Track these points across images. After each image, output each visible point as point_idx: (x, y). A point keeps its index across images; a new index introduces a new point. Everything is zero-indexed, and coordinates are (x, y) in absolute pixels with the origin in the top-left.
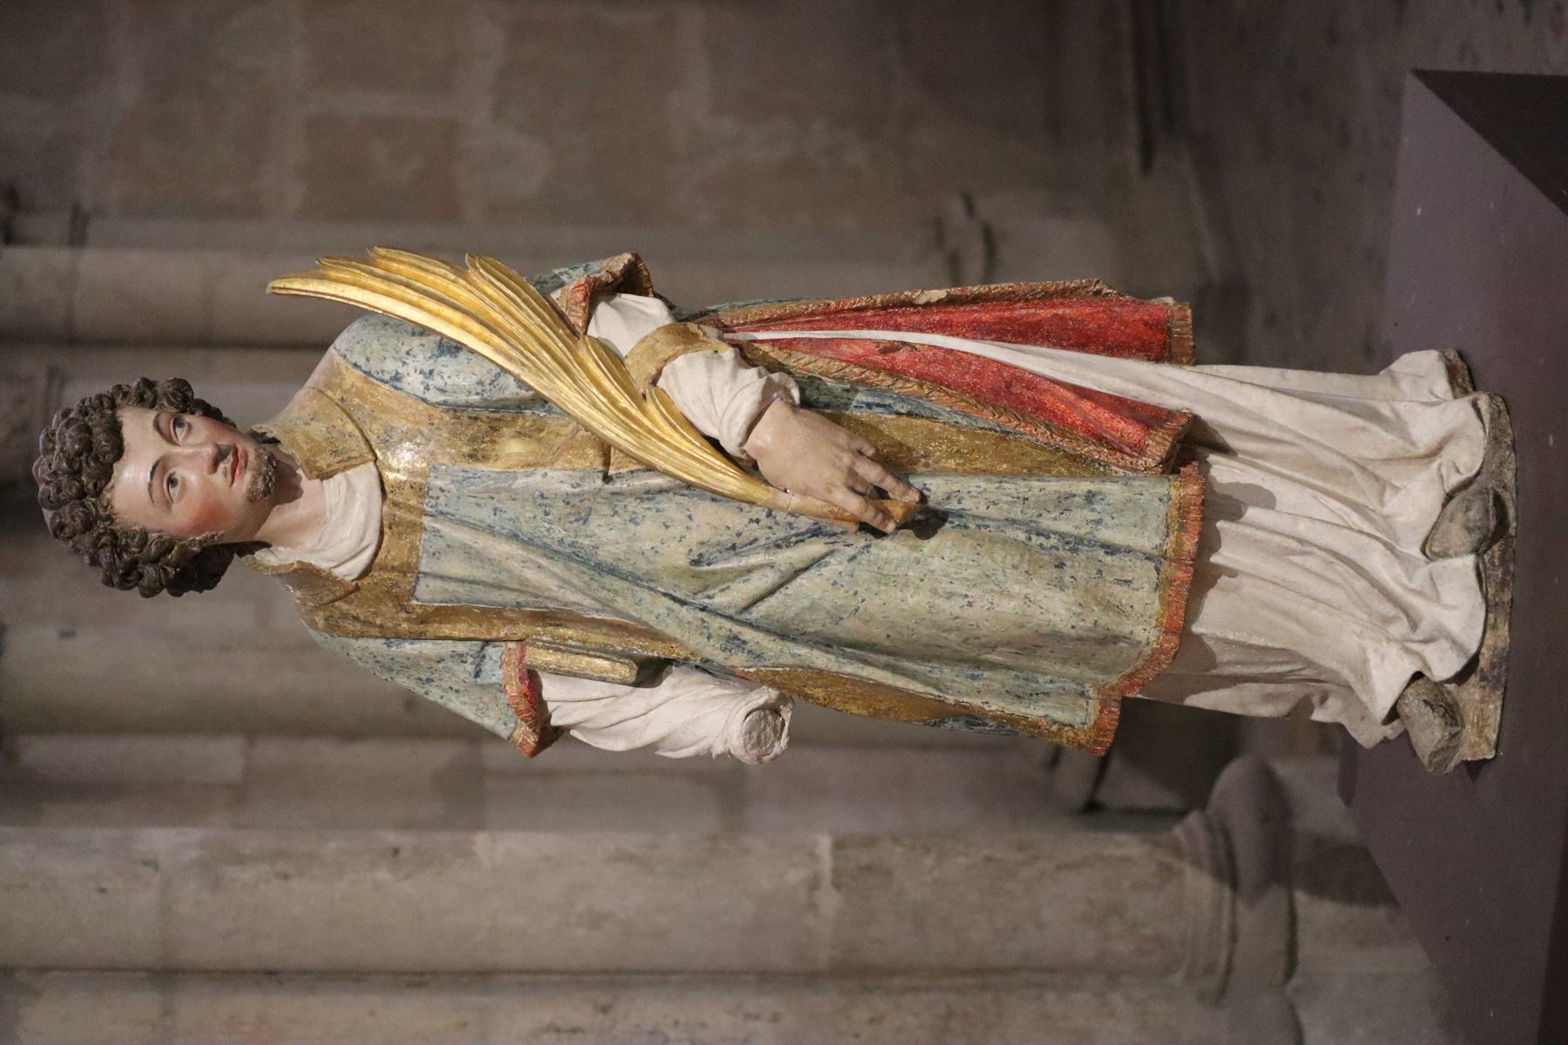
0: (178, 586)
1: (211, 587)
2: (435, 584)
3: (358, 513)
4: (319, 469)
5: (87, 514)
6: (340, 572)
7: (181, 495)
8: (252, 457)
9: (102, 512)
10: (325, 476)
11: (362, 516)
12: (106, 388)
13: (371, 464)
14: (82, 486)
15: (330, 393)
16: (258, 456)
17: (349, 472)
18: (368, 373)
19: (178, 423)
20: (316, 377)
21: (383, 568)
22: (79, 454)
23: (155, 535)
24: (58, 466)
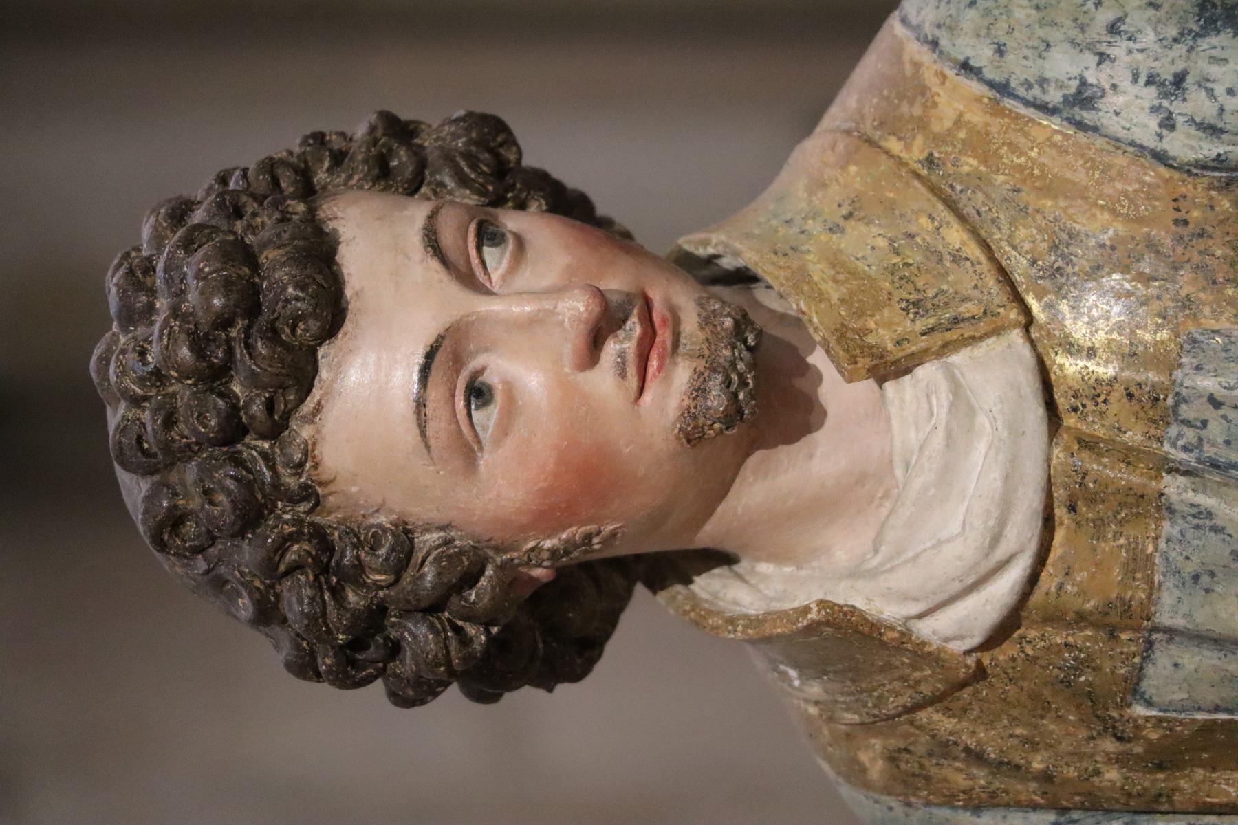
0: (488, 677)
1: (576, 676)
2: (1194, 660)
3: (982, 470)
4: (877, 353)
5: (248, 485)
6: (932, 630)
7: (504, 429)
8: (690, 323)
9: (291, 482)
10: (888, 369)
11: (995, 478)
12: (286, 141)
13: (1016, 336)
14: (234, 409)
15: (894, 145)
16: (708, 321)
17: (958, 359)
18: (1003, 88)
19: (488, 234)
20: (855, 98)
21: (1054, 617)
22: (224, 322)
23: (433, 538)
24: (168, 356)
